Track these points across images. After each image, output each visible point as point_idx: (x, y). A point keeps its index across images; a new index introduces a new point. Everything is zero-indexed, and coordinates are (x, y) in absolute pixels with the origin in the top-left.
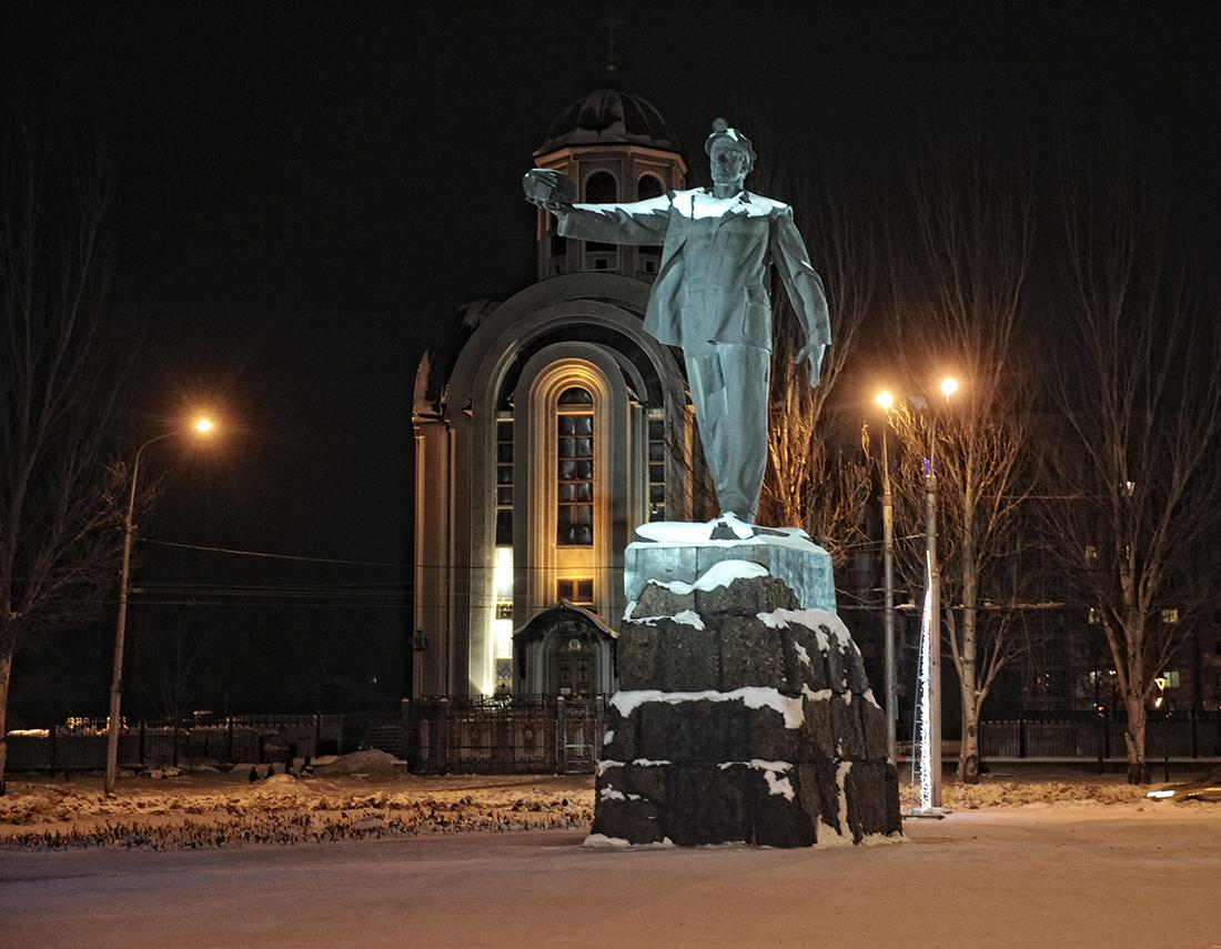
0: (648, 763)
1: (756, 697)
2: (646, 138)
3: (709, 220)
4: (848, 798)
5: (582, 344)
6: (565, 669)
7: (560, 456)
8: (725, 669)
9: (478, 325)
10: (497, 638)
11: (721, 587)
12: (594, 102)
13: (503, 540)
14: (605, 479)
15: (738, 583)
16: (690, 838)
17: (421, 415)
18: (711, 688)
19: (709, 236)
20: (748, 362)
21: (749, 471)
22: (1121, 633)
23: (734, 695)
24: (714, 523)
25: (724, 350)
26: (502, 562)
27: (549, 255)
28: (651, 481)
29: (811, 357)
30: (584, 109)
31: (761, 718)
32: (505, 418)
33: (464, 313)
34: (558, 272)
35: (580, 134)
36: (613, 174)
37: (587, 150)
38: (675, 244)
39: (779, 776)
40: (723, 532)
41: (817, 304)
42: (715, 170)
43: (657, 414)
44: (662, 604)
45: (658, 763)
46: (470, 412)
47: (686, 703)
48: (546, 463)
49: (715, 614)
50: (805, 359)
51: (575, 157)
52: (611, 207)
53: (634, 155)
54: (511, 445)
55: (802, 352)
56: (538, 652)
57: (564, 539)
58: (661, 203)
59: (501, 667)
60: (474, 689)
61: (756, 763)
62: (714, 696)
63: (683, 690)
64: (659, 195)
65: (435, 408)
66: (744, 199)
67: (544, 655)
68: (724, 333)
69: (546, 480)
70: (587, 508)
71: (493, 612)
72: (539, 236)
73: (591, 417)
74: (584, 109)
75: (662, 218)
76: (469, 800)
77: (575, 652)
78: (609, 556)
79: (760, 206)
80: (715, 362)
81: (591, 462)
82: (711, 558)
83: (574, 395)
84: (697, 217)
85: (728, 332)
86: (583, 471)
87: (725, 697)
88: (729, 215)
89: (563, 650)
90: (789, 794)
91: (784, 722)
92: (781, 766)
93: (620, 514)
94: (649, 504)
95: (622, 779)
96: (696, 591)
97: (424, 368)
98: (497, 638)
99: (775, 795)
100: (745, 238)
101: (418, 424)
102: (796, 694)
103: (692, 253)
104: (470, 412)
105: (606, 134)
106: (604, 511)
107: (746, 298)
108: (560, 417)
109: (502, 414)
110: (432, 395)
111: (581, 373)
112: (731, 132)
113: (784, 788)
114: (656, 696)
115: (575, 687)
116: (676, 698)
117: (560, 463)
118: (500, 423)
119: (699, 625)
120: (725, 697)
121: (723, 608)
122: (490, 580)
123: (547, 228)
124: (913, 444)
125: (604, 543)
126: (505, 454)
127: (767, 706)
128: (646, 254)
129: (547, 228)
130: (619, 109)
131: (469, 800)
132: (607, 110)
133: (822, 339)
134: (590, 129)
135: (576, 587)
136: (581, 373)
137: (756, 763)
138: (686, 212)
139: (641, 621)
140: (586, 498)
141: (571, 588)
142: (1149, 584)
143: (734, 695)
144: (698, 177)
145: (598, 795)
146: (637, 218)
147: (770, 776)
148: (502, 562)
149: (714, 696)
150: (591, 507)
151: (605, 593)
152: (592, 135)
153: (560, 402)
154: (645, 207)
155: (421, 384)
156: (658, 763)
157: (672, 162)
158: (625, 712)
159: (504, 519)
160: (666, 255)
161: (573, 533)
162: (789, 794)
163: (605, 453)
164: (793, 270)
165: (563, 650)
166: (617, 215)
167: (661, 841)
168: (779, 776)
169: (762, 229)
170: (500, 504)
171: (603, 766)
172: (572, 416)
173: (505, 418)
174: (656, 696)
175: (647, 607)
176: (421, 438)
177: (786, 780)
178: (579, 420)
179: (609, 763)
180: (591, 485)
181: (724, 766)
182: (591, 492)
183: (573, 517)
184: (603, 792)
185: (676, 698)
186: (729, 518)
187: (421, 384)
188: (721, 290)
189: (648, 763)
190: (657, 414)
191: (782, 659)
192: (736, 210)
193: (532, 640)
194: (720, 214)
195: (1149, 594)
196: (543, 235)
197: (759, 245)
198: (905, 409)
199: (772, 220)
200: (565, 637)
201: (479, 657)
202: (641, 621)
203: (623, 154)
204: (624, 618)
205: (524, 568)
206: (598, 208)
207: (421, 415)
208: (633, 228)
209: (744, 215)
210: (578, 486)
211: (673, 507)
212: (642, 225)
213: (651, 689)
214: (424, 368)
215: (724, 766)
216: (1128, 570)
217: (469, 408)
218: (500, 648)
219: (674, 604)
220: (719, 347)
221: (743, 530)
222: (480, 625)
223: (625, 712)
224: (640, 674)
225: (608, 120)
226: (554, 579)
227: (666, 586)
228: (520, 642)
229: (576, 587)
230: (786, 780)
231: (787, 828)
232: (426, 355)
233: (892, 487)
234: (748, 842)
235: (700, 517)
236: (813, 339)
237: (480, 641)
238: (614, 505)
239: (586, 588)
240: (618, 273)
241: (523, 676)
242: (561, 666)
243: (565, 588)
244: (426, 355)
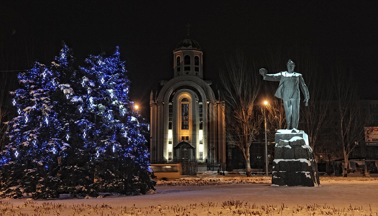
0: (282, 172)
1: (302, 160)
2: (196, 49)
3: (289, 77)
4: (316, 178)
5: (187, 89)
6: (183, 154)
7: (182, 111)
8: (296, 155)
9: (163, 86)
10: (169, 148)
11: (294, 141)
12: (186, 41)
13: (170, 128)
14: (191, 116)
15: (297, 140)
16: (291, 184)
17: (152, 103)
18: (294, 159)
19: (289, 80)
20: (296, 102)
21: (296, 121)
22: (340, 151)
23: (298, 160)
24: (292, 130)
25: (292, 100)
26: (170, 133)
27: (176, 71)
28: (200, 116)
29: (306, 101)
30: (184, 42)
31: (304, 164)
32: (170, 104)
33: (160, 82)
34: (178, 75)
35: (183, 48)
36: (190, 55)
37: (184, 51)
38: (282, 81)
39: (308, 174)
40: (294, 131)
41: (307, 92)
42: (289, 69)
43: (201, 103)
44: (283, 144)
45: (284, 172)
46: (163, 103)
47: (288, 161)
48: (179, 113)
49: (293, 146)
50: (305, 101)
51: (182, 52)
52: (272, 75)
53: (194, 52)
54: (172, 109)
55: (305, 100)
56: (178, 151)
57: (183, 128)
58: (280, 74)
59: (170, 154)
60: (165, 158)
61: (303, 172)
62: (294, 160)
63: (287, 159)
64: (279, 72)
65: (155, 102)
66: (295, 73)
67: (179, 152)
68: (293, 97)
69: (179, 116)
70: (187, 122)
71: (168, 143)
72: (174, 68)
73: (188, 104)
74: (184, 42)
75: (280, 77)
76: (184, 179)
77: (185, 151)
78: (192, 131)
79: (297, 75)
80: (290, 102)
81: (188, 113)
82: (293, 136)
83: (185, 100)
84: (287, 76)
85: (293, 97)
86: (187, 114)
87: (296, 160)
88: (293, 76)
89: (183, 150)
90: (310, 177)
91: (308, 165)
92: (308, 172)
93: (195, 123)
94: (199, 121)
95: (278, 174)
96: (289, 142)
97: (152, 94)
98: (169, 148)
99: (307, 177)
100: (296, 80)
101: (151, 105)
102: (309, 160)
103: (286, 83)
104: (163, 103)
105: (189, 48)
106: (191, 122)
107: (297, 90)
108: (182, 104)
109: (170, 103)
110: (154, 99)
111: (187, 95)
112: (292, 62)
113: (309, 176)
114: (283, 160)
115: (185, 158)
116: (287, 160)
117: (182, 113)
118: (169, 105)
119: (290, 148)
120: (296, 160)
121: (295, 145)
122: (168, 136)
123: (176, 66)
124: (271, 112)
125: (191, 129)
126: (171, 111)
127: (304, 162)
128: (275, 84)
129: (176, 66)
130: (191, 43)
131: (184, 179)
132: (188, 43)
133: (308, 98)
134: (185, 47)
135: (185, 138)
136: (187, 95)
137: (303, 172)
138: (284, 75)
139: (279, 147)
140: (187, 120)
141: (184, 138)
142: (315, 139)
143: (298, 160)
144: (286, 69)
145: (273, 178)
146: (276, 76)
147: (306, 174)
148: (170, 133)
149: (294, 160)
150: (188, 122)
151: (191, 139)
152: (185, 48)
153: (182, 101)
154: (277, 75)
155: (151, 97)
156: (284, 172)
157: (201, 53)
158: (277, 163)
159: (170, 124)
160: (280, 84)
161: (185, 127)
162: (310, 177)
163: (191, 111)
164: (303, 86)
165: (183, 150)
166: (272, 76)
167: (285, 185)
168: (308, 174)
169: (298, 79)
170: (169, 121)
171: (273, 172)
172: (185, 104)
173: (170, 104)
174: (283, 160)
175: (280, 144)
176: (151, 108)
177: (309, 175)
178: (186, 104)
179: (274, 172)
180: (188, 117)
181: (297, 172)
182: (188, 118)
183: (185, 123)
184: (274, 177)
185: (287, 160)
186: (294, 129)
187: (151, 97)
188: (292, 89)
189: (282, 172)
190: (201, 103)
191: (305, 154)
192: (294, 76)
193: (177, 149)
194: (291, 76)
195: (315, 141)
196: (175, 67)
197: (298, 82)
198: (269, 105)
199: (299, 76)
200: (183, 148)
201: (166, 152)
202: (279, 147)
203: (192, 52)
204: (304, 147)
205: (175, 134)
206: (270, 75)
207: (152, 103)
208: (275, 78)
209: (295, 76)
210: (186, 118)
211: (204, 122)
212: (277, 78)
213: (282, 159)
214: (152, 94)
215: (297, 172)
216: (311, 136)
217: (163, 102)
218: (169, 150)
219: (285, 144)
220: (291, 99)
221: (298, 131)
222: (166, 145)
223: (277, 163)
224: (279, 156)
225: (189, 45)
226: (181, 136)
227: (283, 141)
228: (175, 149)
229: (185, 138)
230: (309, 175)
231: (309, 183)
232: (152, 91)
233: (266, 120)
234: (302, 186)
235: (290, 129)
236: (307, 98)
237: (166, 148)
238: (193, 121)
239: (187, 138)
240: (191, 75)
241: (175, 155)
242: (182, 153)
243: (183, 138)
244: (152, 91)
